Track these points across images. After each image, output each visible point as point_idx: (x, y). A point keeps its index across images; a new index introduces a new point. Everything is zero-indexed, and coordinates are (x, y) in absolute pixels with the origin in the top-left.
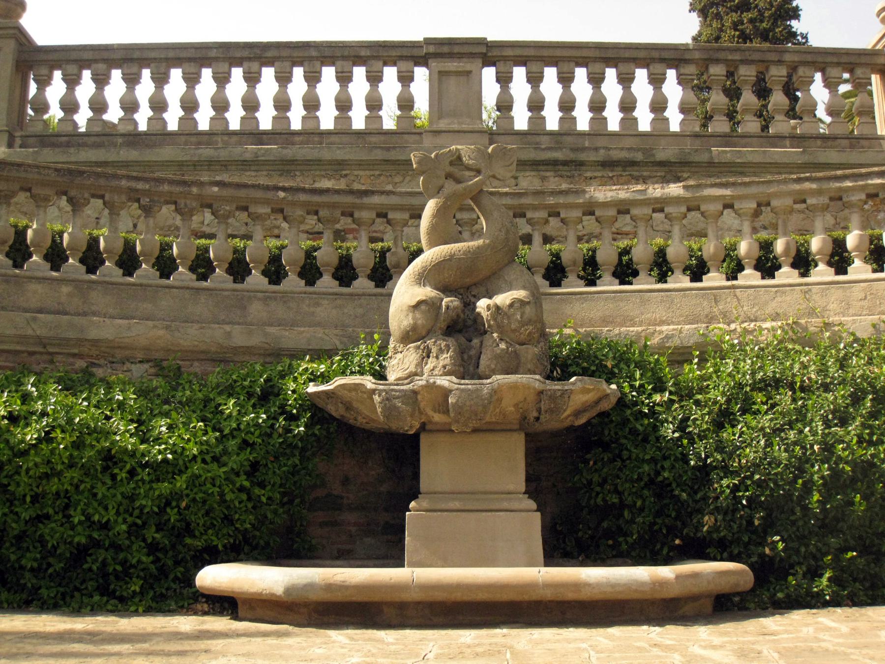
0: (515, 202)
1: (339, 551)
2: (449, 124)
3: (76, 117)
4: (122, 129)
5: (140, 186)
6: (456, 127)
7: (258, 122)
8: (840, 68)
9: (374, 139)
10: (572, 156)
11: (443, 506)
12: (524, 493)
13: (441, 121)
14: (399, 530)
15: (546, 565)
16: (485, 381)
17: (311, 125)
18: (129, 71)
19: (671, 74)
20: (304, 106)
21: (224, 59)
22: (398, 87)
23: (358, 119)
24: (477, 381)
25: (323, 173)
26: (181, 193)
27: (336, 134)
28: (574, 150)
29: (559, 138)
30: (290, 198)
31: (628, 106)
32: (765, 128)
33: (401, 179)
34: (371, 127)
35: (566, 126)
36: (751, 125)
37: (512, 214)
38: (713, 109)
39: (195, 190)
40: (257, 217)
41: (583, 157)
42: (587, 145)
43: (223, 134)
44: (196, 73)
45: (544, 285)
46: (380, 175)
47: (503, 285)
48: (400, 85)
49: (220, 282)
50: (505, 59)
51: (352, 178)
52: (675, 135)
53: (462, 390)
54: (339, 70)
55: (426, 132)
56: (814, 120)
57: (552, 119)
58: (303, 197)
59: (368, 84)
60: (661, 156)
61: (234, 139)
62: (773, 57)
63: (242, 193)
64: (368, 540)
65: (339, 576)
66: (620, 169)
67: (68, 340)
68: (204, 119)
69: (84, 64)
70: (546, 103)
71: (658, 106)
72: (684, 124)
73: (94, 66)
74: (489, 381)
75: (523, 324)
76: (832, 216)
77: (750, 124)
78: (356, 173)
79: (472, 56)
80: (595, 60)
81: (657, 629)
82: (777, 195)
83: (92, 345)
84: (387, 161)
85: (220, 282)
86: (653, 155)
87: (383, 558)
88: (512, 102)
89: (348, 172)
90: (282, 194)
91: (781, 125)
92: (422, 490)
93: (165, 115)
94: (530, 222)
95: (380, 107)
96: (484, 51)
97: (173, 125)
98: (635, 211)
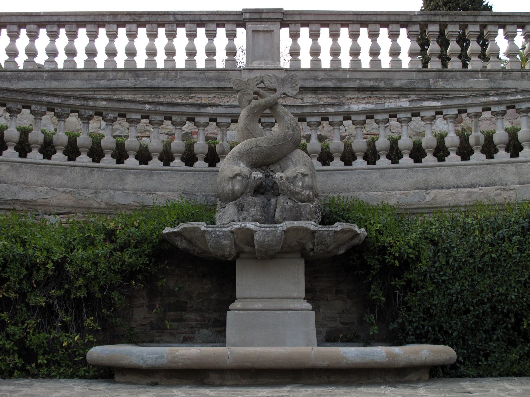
0: (299, 111)
1: (184, 338)
2: (259, 64)
3: (17, 60)
4: (47, 67)
5: (55, 100)
6: (263, 66)
7: (136, 64)
8: (516, 26)
9: (211, 74)
10: (338, 85)
11: (250, 307)
12: (304, 299)
13: (255, 62)
14: (224, 324)
15: (318, 345)
16: (277, 225)
17: (170, 66)
18: (51, 30)
19: (403, 32)
20: (166, 53)
21: (114, 22)
22: (226, 41)
23: (201, 62)
24: (273, 225)
25: (178, 96)
26: (82, 105)
27: (187, 70)
28: (339, 80)
29: (330, 73)
30: (153, 109)
31: (375, 52)
32: (465, 65)
33: (228, 99)
34: (208, 66)
35: (335, 66)
36: (455, 64)
37: (297, 119)
38: (430, 53)
39: (91, 103)
40: (133, 121)
41: (345, 85)
42: (348, 77)
43: (113, 71)
44: (95, 32)
45: (318, 165)
46: (215, 97)
47: (291, 164)
48: (227, 39)
49: (107, 163)
50: (295, 22)
51: (197, 99)
52: (406, 71)
53: (263, 231)
54: (188, 30)
55: (244, 69)
56: (498, 60)
57: (326, 61)
58: (162, 108)
59: (207, 39)
60: (397, 84)
61: (120, 74)
62: (471, 19)
63: (122, 106)
64: (204, 331)
65: (180, 351)
66: (369, 92)
67: (7, 200)
68: (100, 62)
69: (22, 25)
70: (321, 51)
71: (395, 52)
72: (411, 64)
73: (28, 26)
74: (280, 225)
75: (304, 188)
76: (509, 122)
77: (455, 63)
78: (199, 96)
79: (274, 20)
80: (354, 22)
81: (391, 389)
82: (472, 105)
83: (22, 204)
84: (218, 89)
85: (107, 163)
86: (391, 84)
87: (213, 342)
88: (300, 50)
89: (194, 95)
90: (147, 107)
91: (475, 64)
92: (237, 296)
93: (75, 59)
94: (309, 124)
95: (214, 54)
96: (282, 17)
97: (80, 65)
98: (377, 117)
